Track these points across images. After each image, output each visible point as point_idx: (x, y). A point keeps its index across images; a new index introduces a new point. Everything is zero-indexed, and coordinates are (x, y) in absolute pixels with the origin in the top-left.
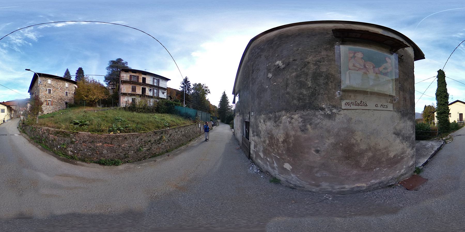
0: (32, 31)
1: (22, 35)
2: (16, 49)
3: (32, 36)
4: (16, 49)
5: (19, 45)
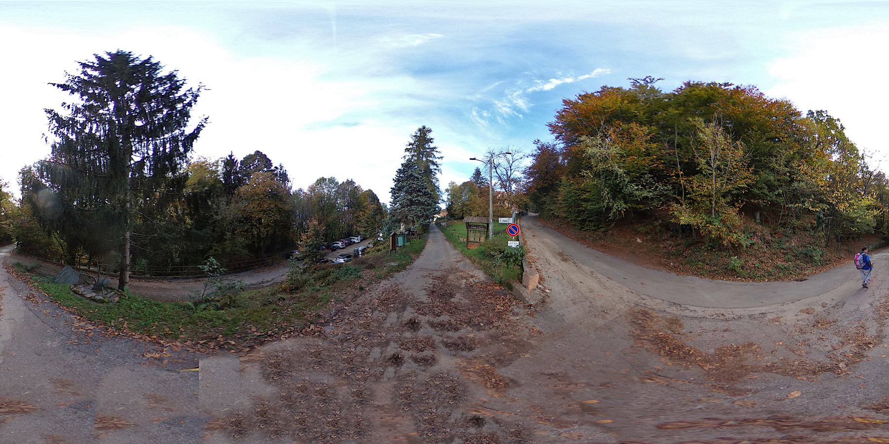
0: (520, 97)
1: (511, 102)
2: (499, 119)
3: (521, 103)
4: (499, 119)
5: (506, 116)
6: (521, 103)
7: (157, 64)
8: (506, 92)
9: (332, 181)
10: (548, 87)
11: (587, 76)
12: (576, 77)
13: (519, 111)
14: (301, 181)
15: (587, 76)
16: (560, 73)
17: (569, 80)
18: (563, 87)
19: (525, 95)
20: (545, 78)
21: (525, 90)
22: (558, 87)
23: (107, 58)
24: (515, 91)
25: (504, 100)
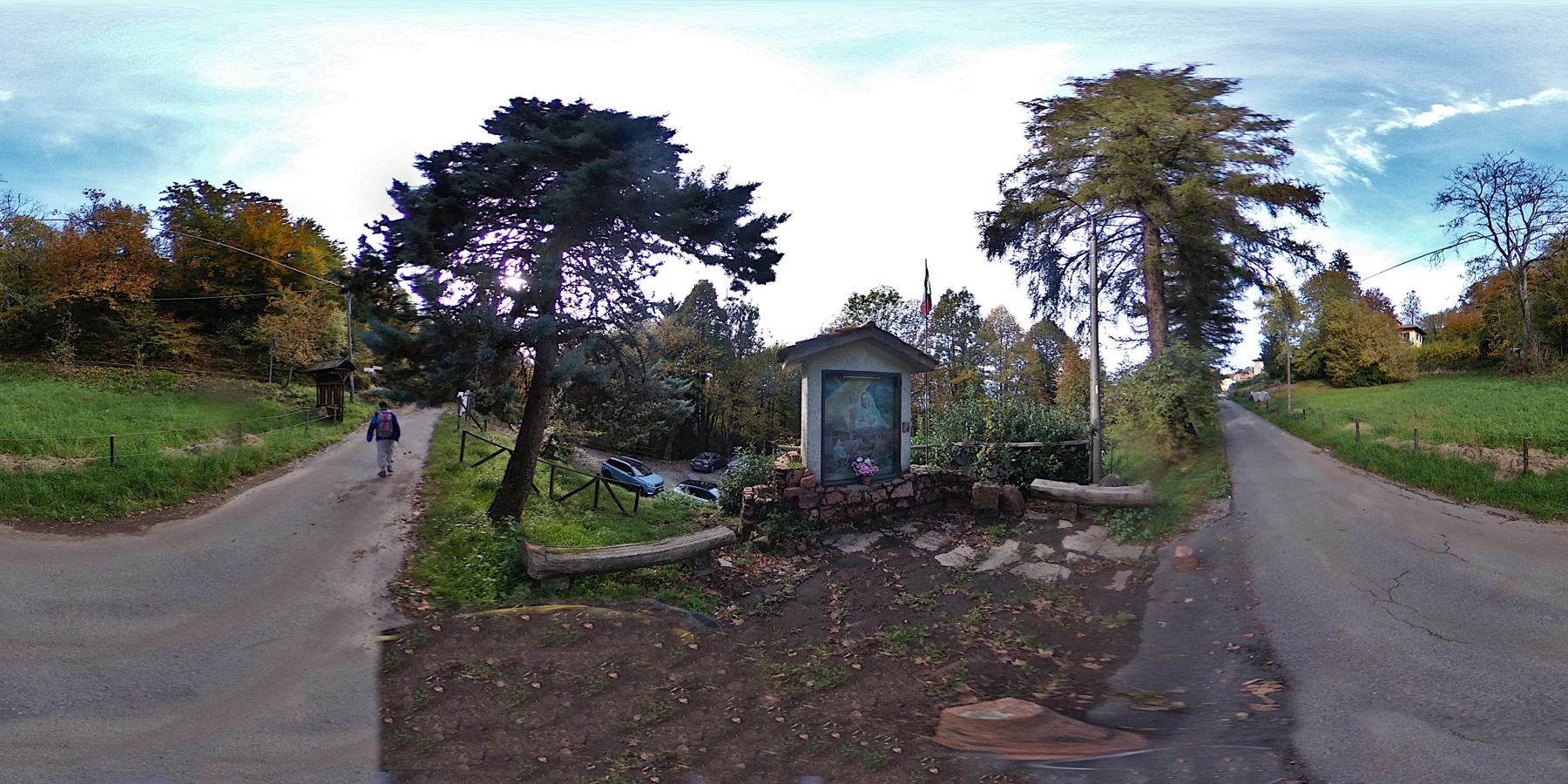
0: (1363, 141)
1: (1341, 153)
3: (1367, 155)
6: (1367, 155)
7: (420, 166)
8: (1331, 133)
9: (467, 145)
10: (1424, 120)
11: (1520, 102)
12: (1494, 103)
13: (1363, 170)
14: (635, 116)
15: (1520, 102)
16: (1455, 95)
17: (1476, 107)
18: (1464, 124)
19: (1373, 137)
20: (1425, 107)
21: (1371, 129)
22: (1446, 127)
23: (418, 180)
24: (1350, 131)
25: (1327, 150)
